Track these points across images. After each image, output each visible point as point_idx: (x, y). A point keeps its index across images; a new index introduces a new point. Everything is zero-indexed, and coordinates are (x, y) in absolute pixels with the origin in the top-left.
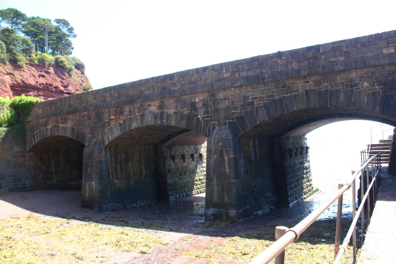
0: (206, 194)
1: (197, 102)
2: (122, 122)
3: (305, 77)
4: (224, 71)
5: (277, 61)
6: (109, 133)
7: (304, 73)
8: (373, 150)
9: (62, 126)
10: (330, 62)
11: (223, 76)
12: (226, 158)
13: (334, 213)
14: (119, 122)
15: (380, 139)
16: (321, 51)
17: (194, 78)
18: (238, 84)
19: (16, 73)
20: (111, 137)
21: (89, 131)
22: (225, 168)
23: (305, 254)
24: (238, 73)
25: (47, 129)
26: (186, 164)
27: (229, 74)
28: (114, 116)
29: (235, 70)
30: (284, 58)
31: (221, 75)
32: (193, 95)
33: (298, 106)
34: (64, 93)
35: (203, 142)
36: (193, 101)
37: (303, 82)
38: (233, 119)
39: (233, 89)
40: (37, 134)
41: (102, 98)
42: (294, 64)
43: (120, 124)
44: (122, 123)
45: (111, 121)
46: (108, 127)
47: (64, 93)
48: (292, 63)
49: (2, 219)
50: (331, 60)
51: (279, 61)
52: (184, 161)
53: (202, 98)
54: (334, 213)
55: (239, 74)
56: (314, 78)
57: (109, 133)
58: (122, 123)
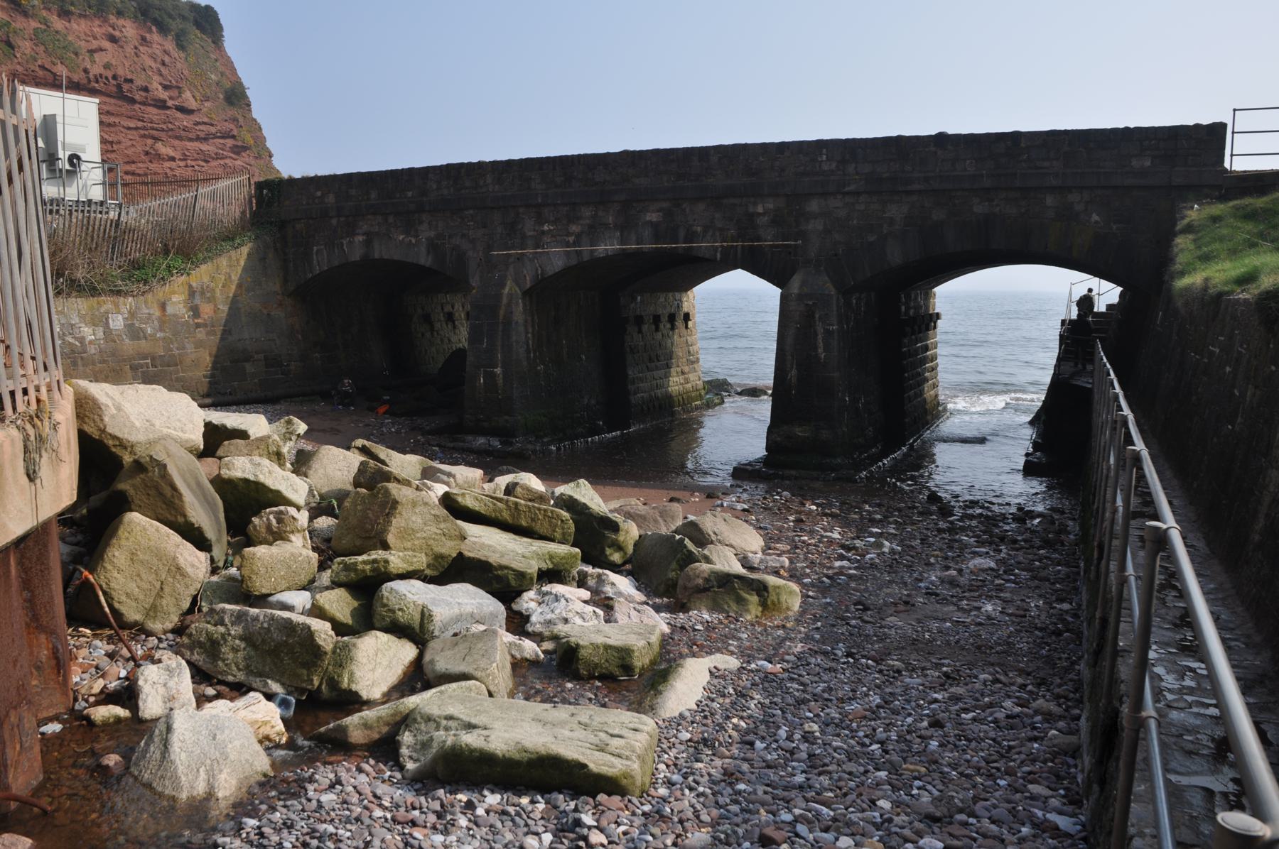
0: (217, 450)
1: (759, 214)
4: (824, 157)
12: (820, 330)
13: (965, 441)
16: (1023, 145)
18: (852, 188)
21: (481, 253)
23: (165, 685)
24: (853, 165)
26: (659, 336)
27: (834, 165)
32: (752, 200)
33: (895, 255)
34: (169, 108)
35: (1188, 289)
36: (751, 210)
39: (839, 197)
47: (169, 108)
52: (657, 329)
53: (771, 206)
54: (965, 441)
55: (856, 168)
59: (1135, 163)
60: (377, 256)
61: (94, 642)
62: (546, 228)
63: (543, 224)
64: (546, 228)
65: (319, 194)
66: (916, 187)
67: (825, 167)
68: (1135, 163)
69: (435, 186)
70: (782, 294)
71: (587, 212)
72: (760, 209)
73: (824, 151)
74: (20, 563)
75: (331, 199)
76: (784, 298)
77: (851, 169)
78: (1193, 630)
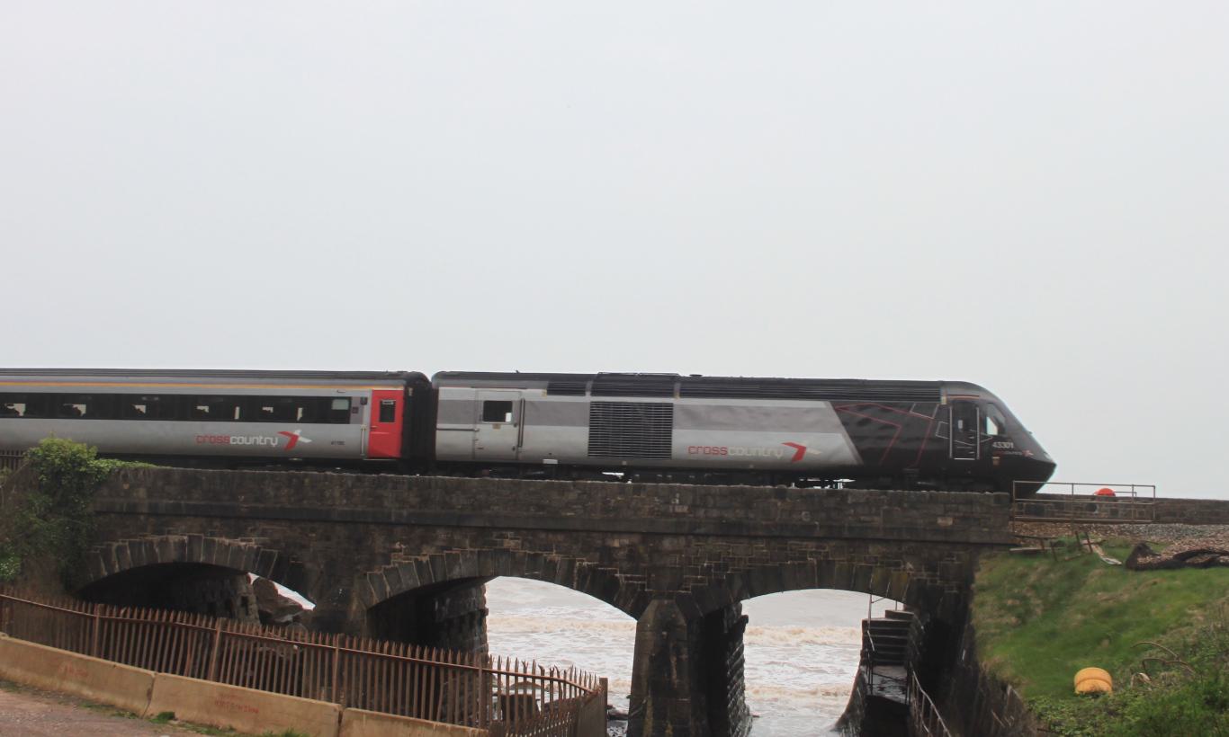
1: (615, 548)
2: (425, 559)
3: (819, 539)
4: (677, 501)
5: (776, 504)
6: (385, 579)
7: (818, 533)
8: (444, 693)
9: (227, 544)
10: (860, 521)
11: (674, 508)
14: (416, 560)
15: (889, 609)
17: (613, 501)
18: (702, 530)
19: (1074, 706)
20: (391, 588)
21: (322, 567)
22: (670, 675)
25: (163, 544)
27: (685, 509)
28: (405, 544)
29: (698, 502)
30: (788, 500)
31: (671, 507)
37: (775, 498)
38: (686, 589)
40: (120, 550)
41: (371, 499)
42: (803, 513)
43: (419, 563)
44: (424, 562)
45: (393, 554)
46: (383, 566)
48: (801, 512)
49: (333, 730)
50: (862, 518)
51: (779, 504)
56: (833, 543)
57: (385, 579)
58: (424, 562)
59: (940, 521)
60: (159, 561)
61: (1158, 538)
62: (397, 546)
63: (394, 542)
64: (397, 546)
65: (126, 486)
66: (760, 533)
67: (678, 510)
68: (940, 521)
69: (272, 493)
70: (638, 623)
71: (442, 534)
72: (616, 544)
73: (678, 495)
74: (1116, 565)
75: (142, 492)
76: (640, 629)
77: (701, 513)
78: (1012, 441)
